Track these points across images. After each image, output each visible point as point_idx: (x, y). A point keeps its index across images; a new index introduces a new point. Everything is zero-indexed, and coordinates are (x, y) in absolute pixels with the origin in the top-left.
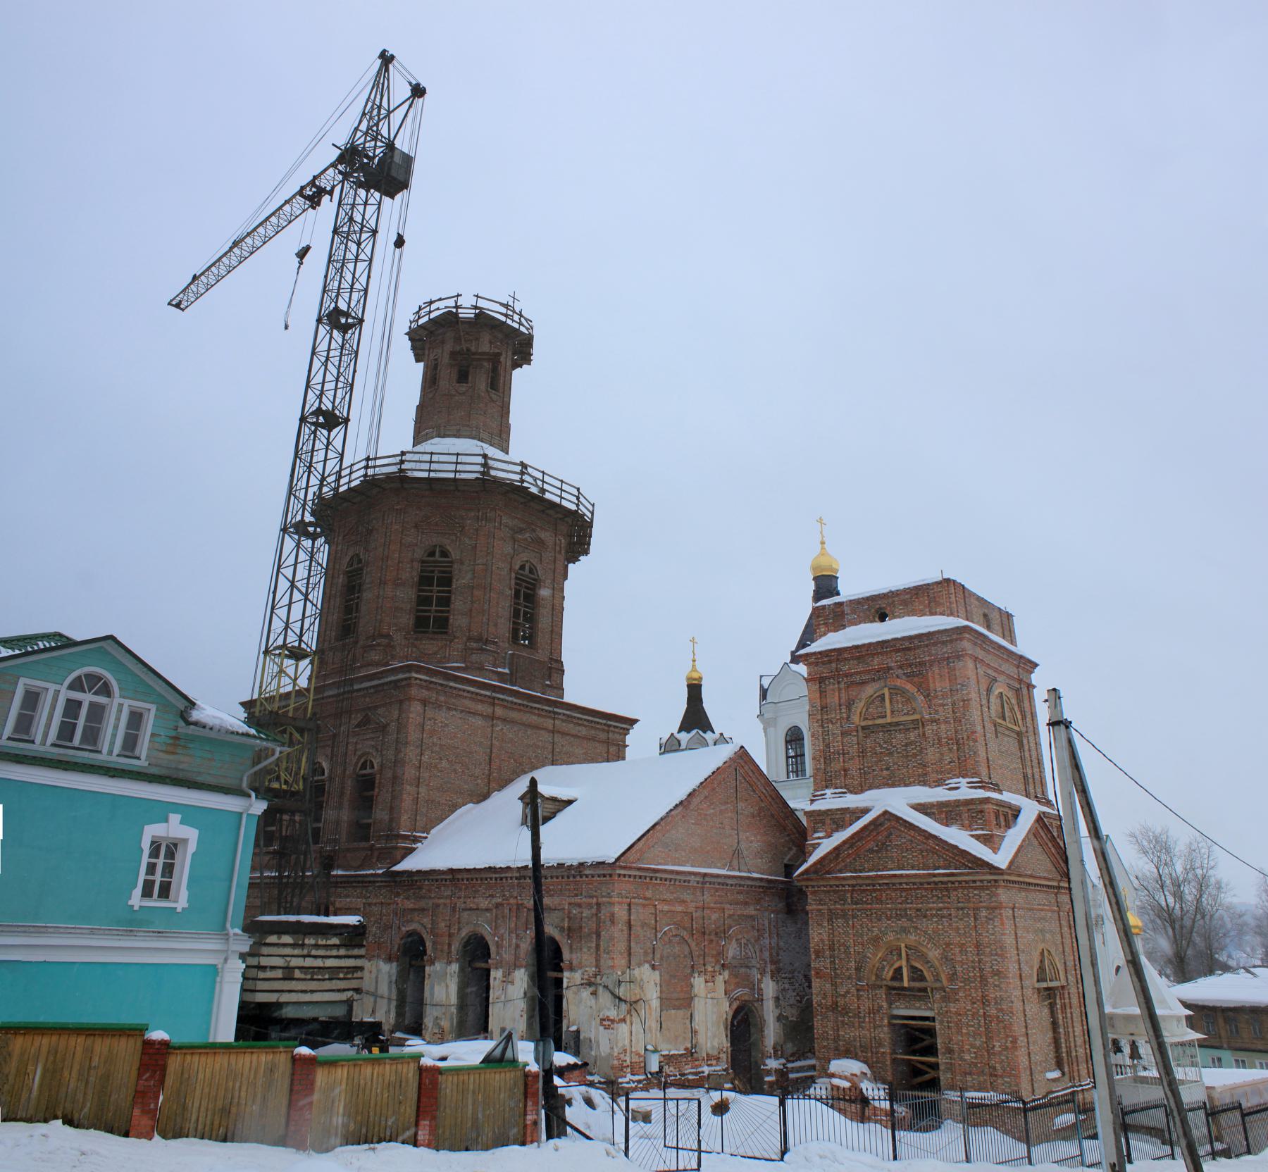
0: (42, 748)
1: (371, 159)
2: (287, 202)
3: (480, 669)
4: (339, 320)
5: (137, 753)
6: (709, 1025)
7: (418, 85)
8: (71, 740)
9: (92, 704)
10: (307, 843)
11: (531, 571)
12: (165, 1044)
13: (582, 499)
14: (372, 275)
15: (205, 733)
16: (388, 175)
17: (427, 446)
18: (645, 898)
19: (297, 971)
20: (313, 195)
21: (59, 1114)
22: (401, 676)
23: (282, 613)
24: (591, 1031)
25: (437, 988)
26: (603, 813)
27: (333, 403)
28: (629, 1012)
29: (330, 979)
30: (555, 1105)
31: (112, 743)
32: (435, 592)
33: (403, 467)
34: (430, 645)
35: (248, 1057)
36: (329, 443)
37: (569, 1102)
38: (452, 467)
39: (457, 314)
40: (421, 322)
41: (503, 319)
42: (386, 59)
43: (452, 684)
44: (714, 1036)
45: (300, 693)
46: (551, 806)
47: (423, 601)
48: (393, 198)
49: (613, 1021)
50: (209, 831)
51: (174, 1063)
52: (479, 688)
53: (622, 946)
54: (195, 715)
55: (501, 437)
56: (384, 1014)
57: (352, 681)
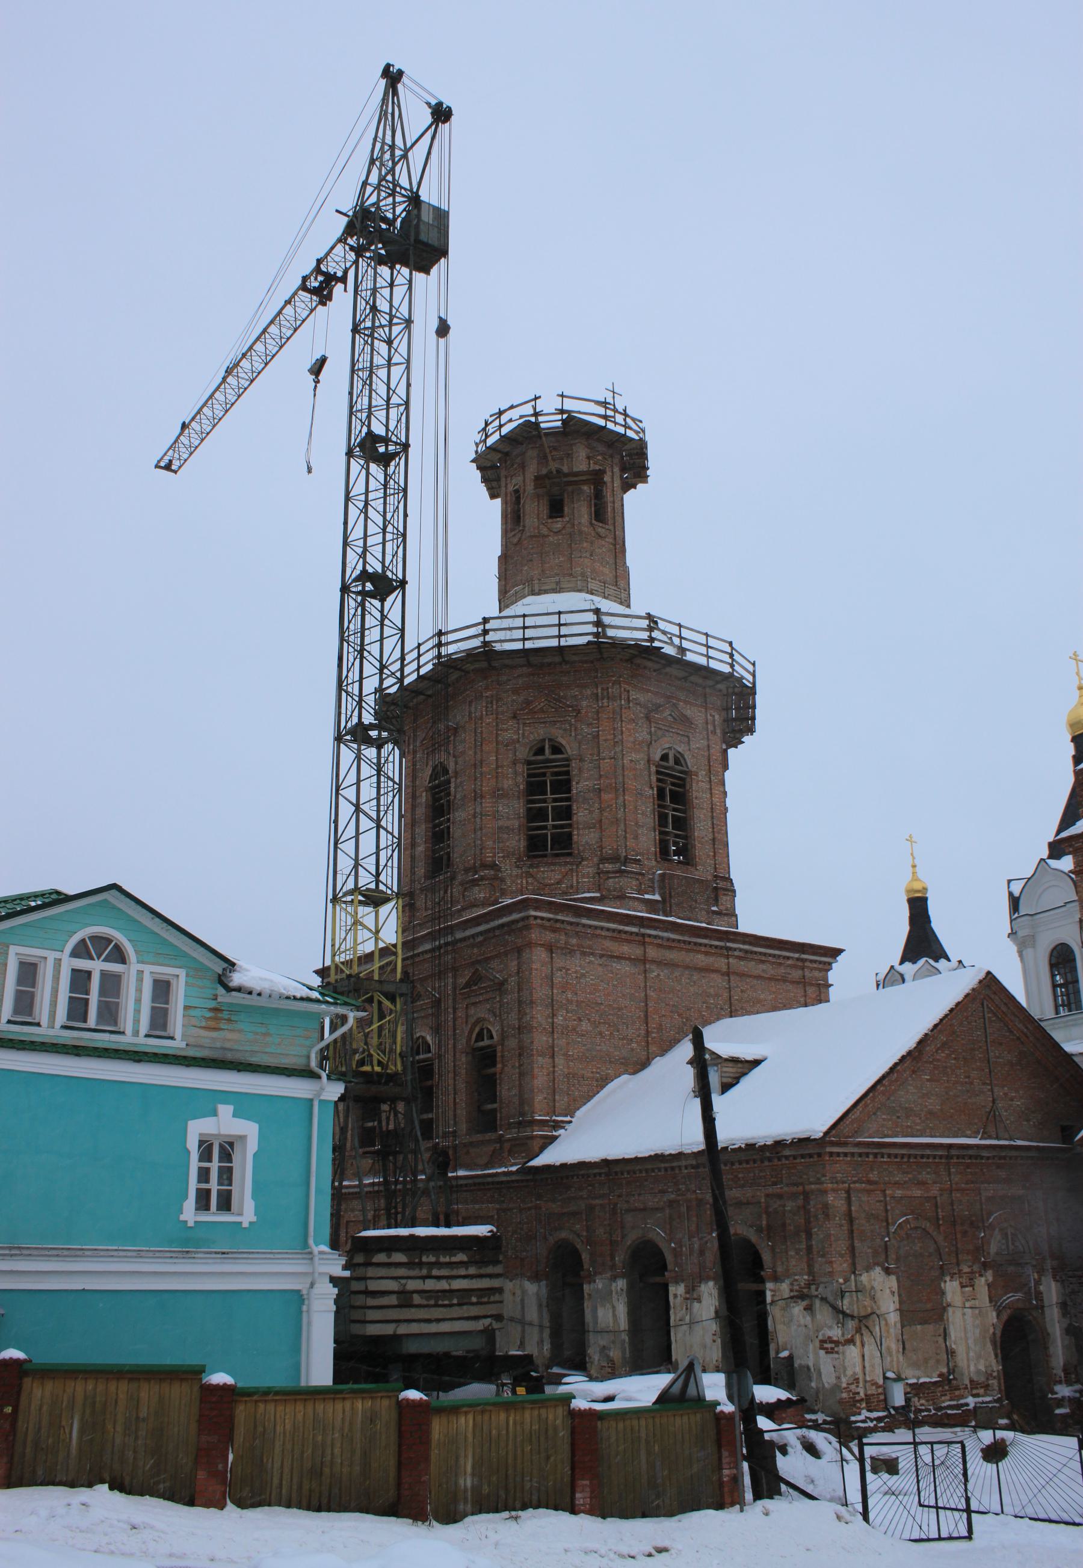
0: (51, 1032)
1: (391, 223)
2: (288, 302)
3: (621, 897)
4: (375, 450)
5: (170, 1032)
6: (970, 1342)
7: (440, 104)
8: (85, 1021)
9: (104, 974)
10: (417, 1141)
11: (677, 762)
12: (225, 1388)
13: (737, 657)
14: (412, 382)
15: (252, 1000)
16: (418, 241)
17: (518, 608)
18: (870, 1182)
19: (415, 1296)
20: (321, 286)
21: (107, 1477)
22: (515, 916)
23: (349, 847)
24: (810, 1356)
25: (601, 1312)
26: (801, 1076)
27: (383, 563)
28: (858, 1330)
29: (459, 1305)
30: (763, 1457)
31: (137, 1021)
32: (549, 801)
33: (488, 638)
34: (550, 873)
35: (339, 1405)
36: (384, 617)
37: (784, 1450)
38: (554, 631)
39: (537, 424)
40: (490, 441)
41: (601, 422)
42: (392, 77)
43: (585, 921)
44: (979, 1357)
45: (386, 951)
46: (731, 1070)
47: (535, 815)
48: (427, 272)
49: (837, 1343)
50: (277, 1127)
51: (241, 1412)
52: (621, 923)
53: (842, 1246)
54: (237, 979)
55: (617, 584)
56: (536, 1345)
57: (451, 929)
